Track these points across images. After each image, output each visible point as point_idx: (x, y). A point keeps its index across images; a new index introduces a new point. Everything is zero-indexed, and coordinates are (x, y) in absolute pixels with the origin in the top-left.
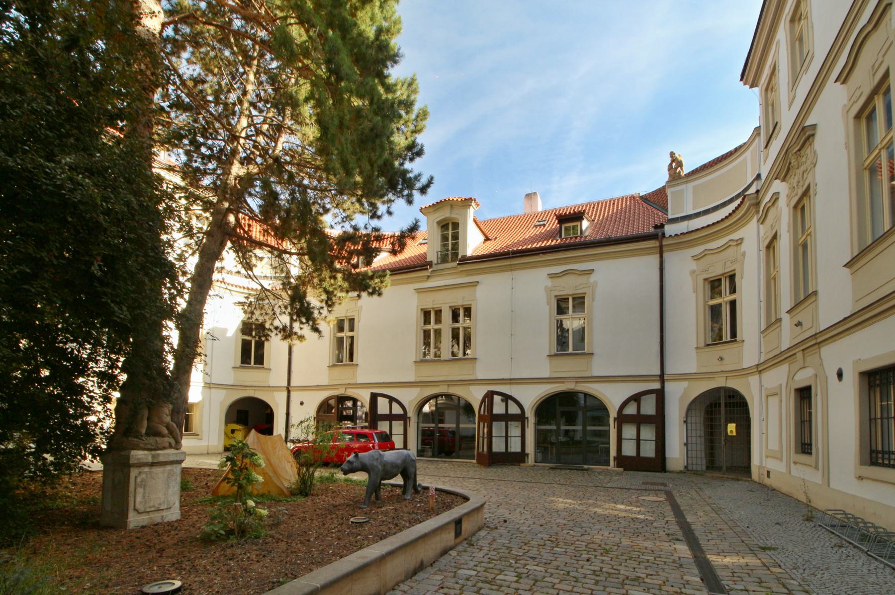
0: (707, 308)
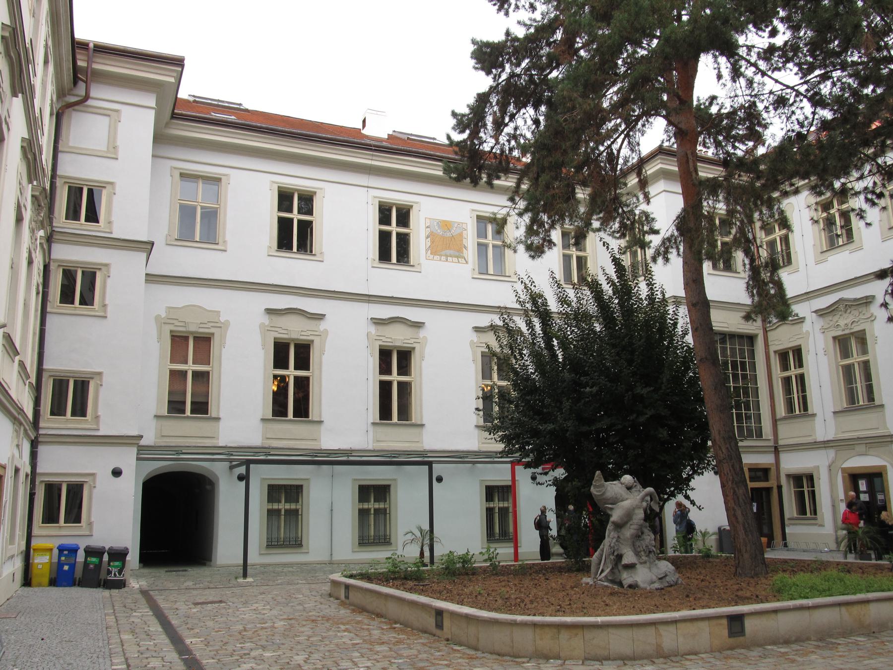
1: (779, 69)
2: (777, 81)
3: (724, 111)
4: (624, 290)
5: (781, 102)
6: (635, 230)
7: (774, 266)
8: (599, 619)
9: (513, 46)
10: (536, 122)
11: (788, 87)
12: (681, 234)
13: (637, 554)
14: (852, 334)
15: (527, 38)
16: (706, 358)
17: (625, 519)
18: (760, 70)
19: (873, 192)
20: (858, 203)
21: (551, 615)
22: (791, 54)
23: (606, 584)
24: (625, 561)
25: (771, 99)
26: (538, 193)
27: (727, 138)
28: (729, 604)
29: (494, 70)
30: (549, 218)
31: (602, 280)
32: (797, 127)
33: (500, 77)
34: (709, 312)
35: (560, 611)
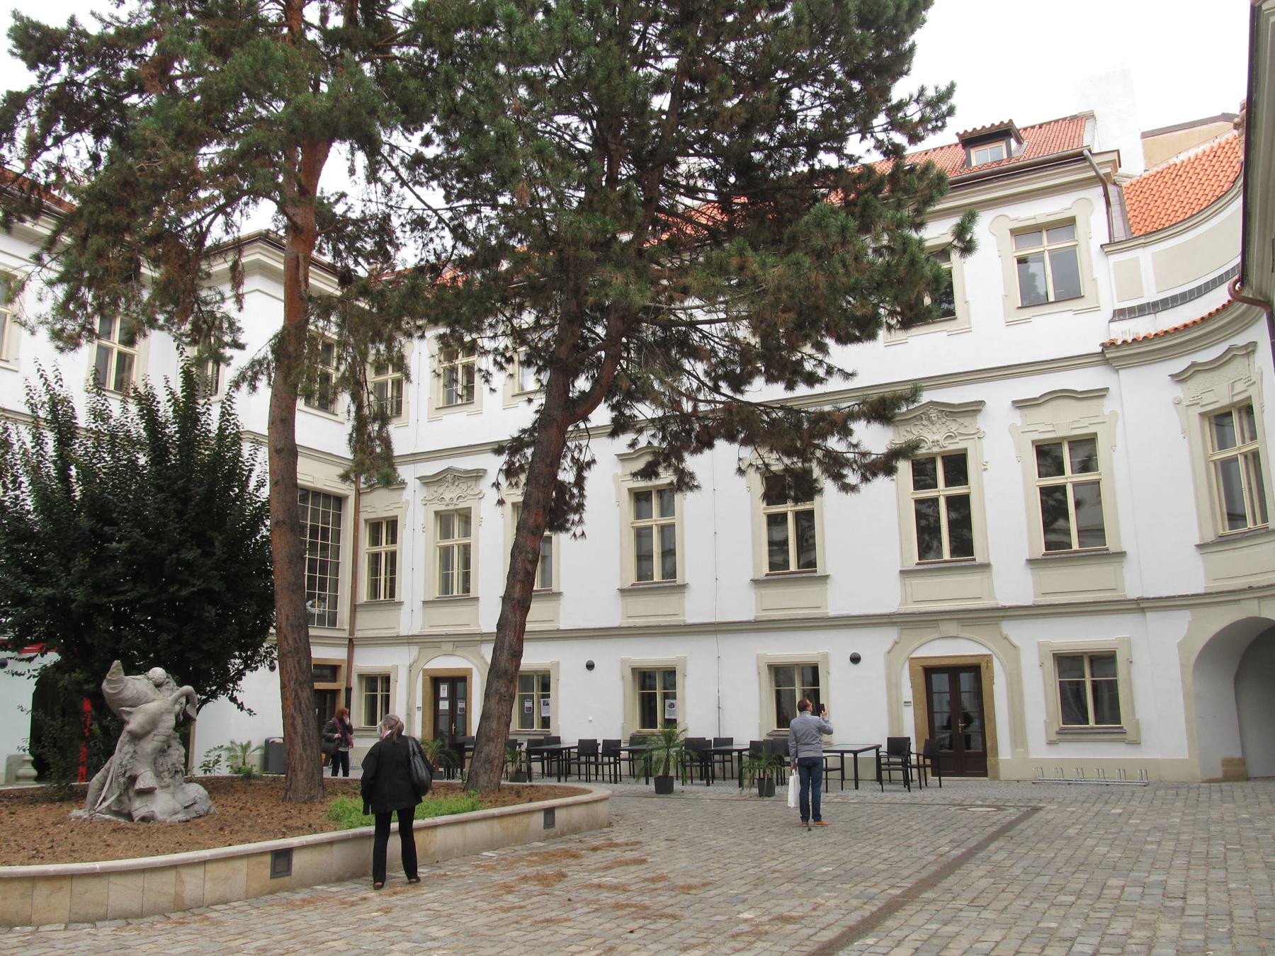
0: (1212, 466)
1: (421, 184)
2: (418, 197)
3: (351, 215)
4: (188, 414)
5: (419, 224)
6: (209, 336)
7: (384, 419)
8: (98, 865)
9: (77, 41)
10: (95, 158)
11: (430, 208)
12: (277, 360)
13: (158, 775)
14: (456, 510)
15: (102, 39)
16: (284, 522)
17: (148, 728)
18: (401, 178)
19: (503, 355)
20: (485, 363)
21: (21, 864)
22: (437, 171)
23: (108, 817)
24: (140, 785)
25: (409, 217)
26: (83, 261)
27: (349, 249)
28: (275, 837)
29: (42, 66)
30: (95, 298)
31: (162, 396)
32: (432, 259)
33: (49, 77)
34: (295, 463)
35: (37, 857)
